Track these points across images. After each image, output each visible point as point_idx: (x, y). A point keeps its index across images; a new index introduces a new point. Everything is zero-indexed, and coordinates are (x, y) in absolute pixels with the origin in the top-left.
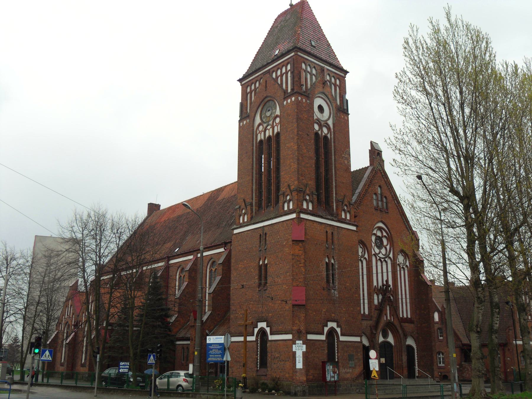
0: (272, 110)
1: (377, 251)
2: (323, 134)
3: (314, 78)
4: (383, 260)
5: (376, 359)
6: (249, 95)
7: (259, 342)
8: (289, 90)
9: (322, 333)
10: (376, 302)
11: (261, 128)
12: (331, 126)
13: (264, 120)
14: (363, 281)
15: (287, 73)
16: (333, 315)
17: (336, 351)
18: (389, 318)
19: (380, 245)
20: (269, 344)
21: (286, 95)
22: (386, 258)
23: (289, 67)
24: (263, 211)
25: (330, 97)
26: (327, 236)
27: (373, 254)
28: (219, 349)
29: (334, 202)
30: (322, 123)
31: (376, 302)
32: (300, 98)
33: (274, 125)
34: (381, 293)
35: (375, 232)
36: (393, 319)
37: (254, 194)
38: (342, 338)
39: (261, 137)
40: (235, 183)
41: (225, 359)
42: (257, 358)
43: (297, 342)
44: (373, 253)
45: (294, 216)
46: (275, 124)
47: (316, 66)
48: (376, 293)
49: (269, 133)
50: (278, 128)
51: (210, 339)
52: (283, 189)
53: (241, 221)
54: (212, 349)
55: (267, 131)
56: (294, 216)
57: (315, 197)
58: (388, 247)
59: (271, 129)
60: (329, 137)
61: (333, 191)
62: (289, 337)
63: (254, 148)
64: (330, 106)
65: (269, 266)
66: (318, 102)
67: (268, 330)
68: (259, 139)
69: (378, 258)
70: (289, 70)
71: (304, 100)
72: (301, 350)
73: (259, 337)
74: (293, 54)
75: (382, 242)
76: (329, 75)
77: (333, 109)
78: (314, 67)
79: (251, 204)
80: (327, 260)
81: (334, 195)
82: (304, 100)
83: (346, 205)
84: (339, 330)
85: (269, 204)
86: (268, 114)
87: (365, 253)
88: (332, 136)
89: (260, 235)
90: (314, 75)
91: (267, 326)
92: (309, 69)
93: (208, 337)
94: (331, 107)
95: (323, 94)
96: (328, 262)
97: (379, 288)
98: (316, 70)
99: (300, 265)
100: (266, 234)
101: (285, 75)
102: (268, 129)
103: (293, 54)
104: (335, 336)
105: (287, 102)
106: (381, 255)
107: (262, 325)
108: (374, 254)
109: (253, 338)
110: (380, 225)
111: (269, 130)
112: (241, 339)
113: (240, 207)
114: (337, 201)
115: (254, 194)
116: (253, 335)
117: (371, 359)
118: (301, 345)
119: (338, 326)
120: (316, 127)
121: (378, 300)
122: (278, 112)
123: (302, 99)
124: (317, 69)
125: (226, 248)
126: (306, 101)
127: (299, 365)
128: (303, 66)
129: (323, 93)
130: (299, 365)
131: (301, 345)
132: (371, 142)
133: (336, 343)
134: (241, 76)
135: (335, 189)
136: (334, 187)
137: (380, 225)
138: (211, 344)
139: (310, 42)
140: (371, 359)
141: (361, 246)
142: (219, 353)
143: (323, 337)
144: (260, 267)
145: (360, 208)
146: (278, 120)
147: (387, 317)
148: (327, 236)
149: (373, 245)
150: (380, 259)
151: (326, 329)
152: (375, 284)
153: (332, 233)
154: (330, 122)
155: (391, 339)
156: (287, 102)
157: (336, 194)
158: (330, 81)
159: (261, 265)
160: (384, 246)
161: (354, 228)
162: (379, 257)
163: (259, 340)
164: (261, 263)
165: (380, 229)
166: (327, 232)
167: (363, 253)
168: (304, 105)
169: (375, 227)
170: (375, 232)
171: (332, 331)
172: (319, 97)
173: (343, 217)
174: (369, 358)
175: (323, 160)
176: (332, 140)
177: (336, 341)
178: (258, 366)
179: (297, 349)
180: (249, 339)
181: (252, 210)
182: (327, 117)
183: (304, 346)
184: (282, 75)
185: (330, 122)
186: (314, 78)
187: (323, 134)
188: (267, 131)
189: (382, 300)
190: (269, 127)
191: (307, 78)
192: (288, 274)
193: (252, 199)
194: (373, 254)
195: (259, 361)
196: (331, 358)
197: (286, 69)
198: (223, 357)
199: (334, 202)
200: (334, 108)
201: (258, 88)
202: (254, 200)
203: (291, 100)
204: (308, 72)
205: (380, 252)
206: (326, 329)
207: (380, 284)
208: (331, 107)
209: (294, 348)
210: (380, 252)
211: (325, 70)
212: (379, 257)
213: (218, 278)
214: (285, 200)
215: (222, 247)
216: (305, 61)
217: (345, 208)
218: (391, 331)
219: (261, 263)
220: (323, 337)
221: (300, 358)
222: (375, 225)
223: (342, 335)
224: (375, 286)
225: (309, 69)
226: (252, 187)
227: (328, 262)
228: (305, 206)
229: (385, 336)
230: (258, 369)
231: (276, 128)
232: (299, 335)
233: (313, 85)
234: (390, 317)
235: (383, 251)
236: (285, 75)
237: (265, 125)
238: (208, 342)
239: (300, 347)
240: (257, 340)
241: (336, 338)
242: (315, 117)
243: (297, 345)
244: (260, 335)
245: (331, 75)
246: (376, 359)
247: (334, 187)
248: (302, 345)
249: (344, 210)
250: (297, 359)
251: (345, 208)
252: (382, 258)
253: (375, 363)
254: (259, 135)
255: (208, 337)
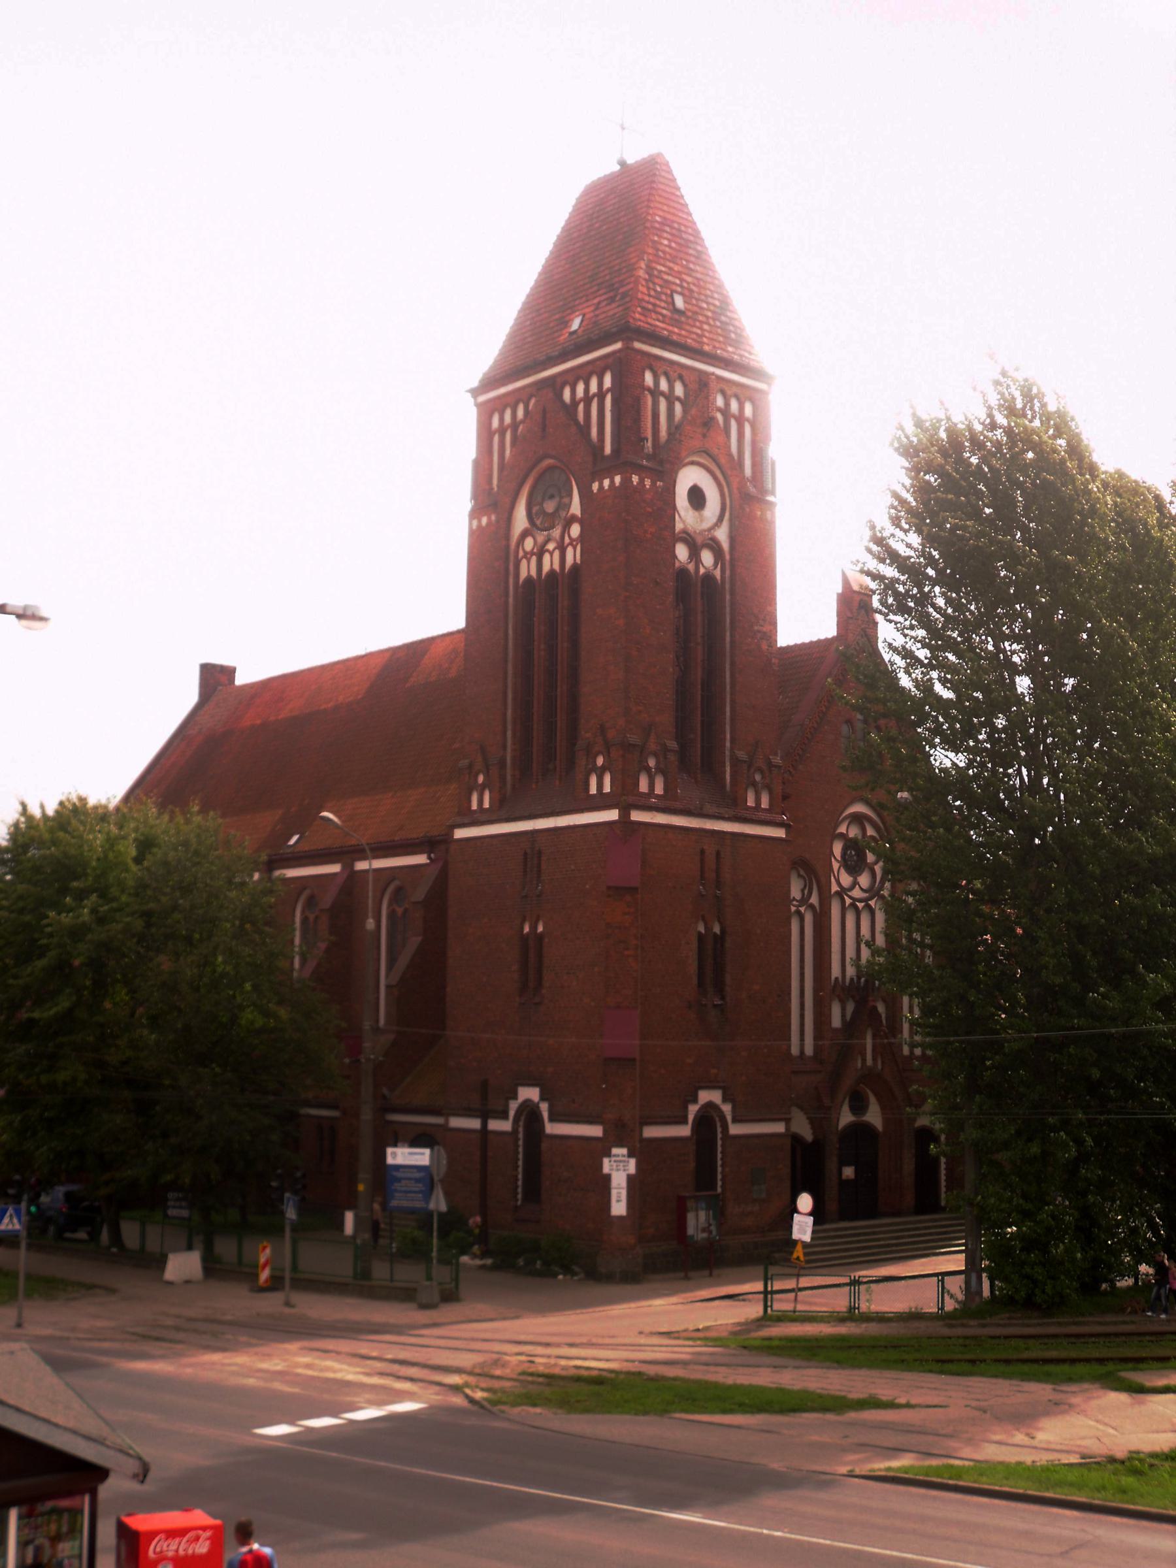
0: (561, 498)
1: (846, 879)
2: (702, 571)
3: (678, 408)
4: (860, 905)
5: (810, 1214)
6: (496, 438)
7: (521, 1136)
8: (608, 450)
9: (683, 1120)
10: (836, 1022)
11: (529, 544)
12: (725, 545)
13: (538, 522)
14: (802, 975)
15: (601, 395)
16: (714, 1071)
17: (719, 1163)
18: (869, 1062)
19: (854, 865)
20: (544, 1146)
21: (600, 465)
22: (871, 898)
23: (608, 381)
24: (534, 786)
25: (723, 461)
26: (702, 861)
27: (833, 891)
28: (417, 1180)
29: (728, 764)
30: (699, 540)
31: (836, 1022)
32: (635, 479)
33: (565, 545)
34: (853, 997)
35: (842, 829)
36: (883, 1063)
37: (509, 734)
38: (735, 1130)
39: (527, 569)
40: (459, 632)
41: (432, 1206)
42: (517, 1176)
43: (615, 1151)
44: (835, 888)
45: (612, 815)
46: (567, 540)
47: (684, 373)
48: (838, 996)
49: (550, 563)
50: (575, 552)
51: (394, 1155)
52: (588, 735)
53: (474, 806)
54: (399, 1180)
55: (547, 557)
56: (612, 815)
57: (672, 757)
58: (878, 869)
59: (557, 554)
60: (718, 577)
61: (724, 733)
62: (595, 1131)
63: (511, 600)
64: (724, 484)
65: (546, 940)
66: (689, 477)
67: (544, 1107)
68: (523, 574)
69: (848, 901)
70: (608, 390)
71: (648, 483)
72: (624, 1170)
73: (521, 1123)
74: (618, 346)
75: (862, 857)
76: (723, 393)
77: (730, 496)
78: (681, 378)
79: (502, 764)
80: (701, 929)
81: (728, 744)
82: (648, 483)
83: (760, 770)
84: (727, 1109)
85: (551, 766)
86: (550, 507)
87: (810, 894)
88: (728, 573)
89: (526, 854)
90: (678, 399)
91: (543, 1098)
92: (664, 385)
93: (389, 1150)
94: (726, 490)
95: (705, 455)
96: (703, 932)
97: (847, 984)
98: (685, 385)
99: (626, 953)
100: (540, 853)
101: (595, 400)
102: (548, 551)
103: (618, 346)
104: (718, 1125)
105: (601, 487)
106: (856, 893)
107: (529, 1093)
108: (837, 893)
109: (505, 1126)
110: (859, 808)
111: (551, 554)
112: (475, 1124)
113: (470, 766)
114: (735, 762)
115: (509, 734)
116: (504, 1115)
117: (798, 1212)
118: (624, 1159)
119: (725, 1099)
120: (682, 552)
121: (843, 1016)
122: (576, 508)
123: (642, 481)
124: (687, 382)
125: (432, 855)
126: (653, 484)
127: (619, 1208)
128: (649, 378)
129: (705, 452)
130: (619, 1208)
131: (624, 1159)
132: (842, 570)
133: (719, 1142)
134: (475, 383)
135: (731, 727)
136: (728, 720)
137: (859, 808)
138: (398, 1167)
139: (670, 300)
140: (798, 1212)
141: (802, 872)
142: (417, 1189)
143: (684, 1131)
144: (524, 939)
145: (800, 767)
146: (575, 530)
147: (864, 1060)
148: (702, 861)
149: (836, 865)
150: (853, 905)
151: (693, 1109)
152: (836, 972)
153: (718, 853)
154: (722, 535)
155: (874, 1116)
156: (601, 487)
157: (733, 740)
158: (725, 412)
159: (528, 934)
160: (866, 864)
161: (780, 833)
162: (850, 897)
163: (521, 1129)
164: (527, 929)
165: (858, 819)
166: (703, 852)
167: (806, 892)
168: (648, 496)
169: (844, 815)
170: (842, 829)
171: (707, 1120)
172: (692, 463)
173: (751, 802)
174: (795, 1210)
175: (700, 647)
176: (727, 586)
177: (719, 1136)
178: (520, 1196)
179: (615, 1167)
180: (495, 1125)
181: (503, 779)
182: (714, 520)
183: (632, 1162)
184: (588, 399)
185: (722, 535)
186: (678, 408)
187: (702, 571)
188: (546, 558)
189: (854, 1013)
190: (551, 546)
191: (659, 415)
192: (596, 969)
193: (504, 747)
194: (833, 891)
195: (520, 1183)
196: (704, 1176)
197: (600, 384)
198: (427, 1201)
199: (728, 764)
200: (735, 491)
201: (522, 422)
202: (509, 750)
203: (612, 482)
204: (662, 394)
205: (855, 883)
206: (693, 1109)
207: (851, 971)
208: (726, 490)
209: (607, 1166)
210: (855, 883)
211: (713, 385)
212: (850, 897)
213: (414, 942)
214: (590, 766)
215: (421, 852)
216: (653, 363)
217: (758, 777)
218: (876, 1095)
219: (527, 929)
220: (684, 1131)
221: (621, 1190)
222: (842, 813)
223: (552, 1119)
224: (837, 979)
225: (664, 385)
226: (505, 714)
227: (703, 932)
228: (643, 786)
229: (859, 1105)
230: (519, 1203)
231: (570, 552)
232: (620, 1133)
233: (675, 430)
234: (874, 1059)
235: (864, 880)
236: (595, 400)
237: (540, 539)
238: (390, 1160)
239: (622, 1164)
240: (515, 1131)
241: (719, 1130)
242: (679, 526)
243: (613, 1159)
244: (523, 1118)
245: (729, 392)
246: (810, 1214)
247: (728, 720)
248: (625, 1159)
249: (754, 784)
250: (614, 1193)
251: (758, 777)
252: (860, 901)
253: (807, 1223)
254: (524, 563)
255: (389, 1150)
